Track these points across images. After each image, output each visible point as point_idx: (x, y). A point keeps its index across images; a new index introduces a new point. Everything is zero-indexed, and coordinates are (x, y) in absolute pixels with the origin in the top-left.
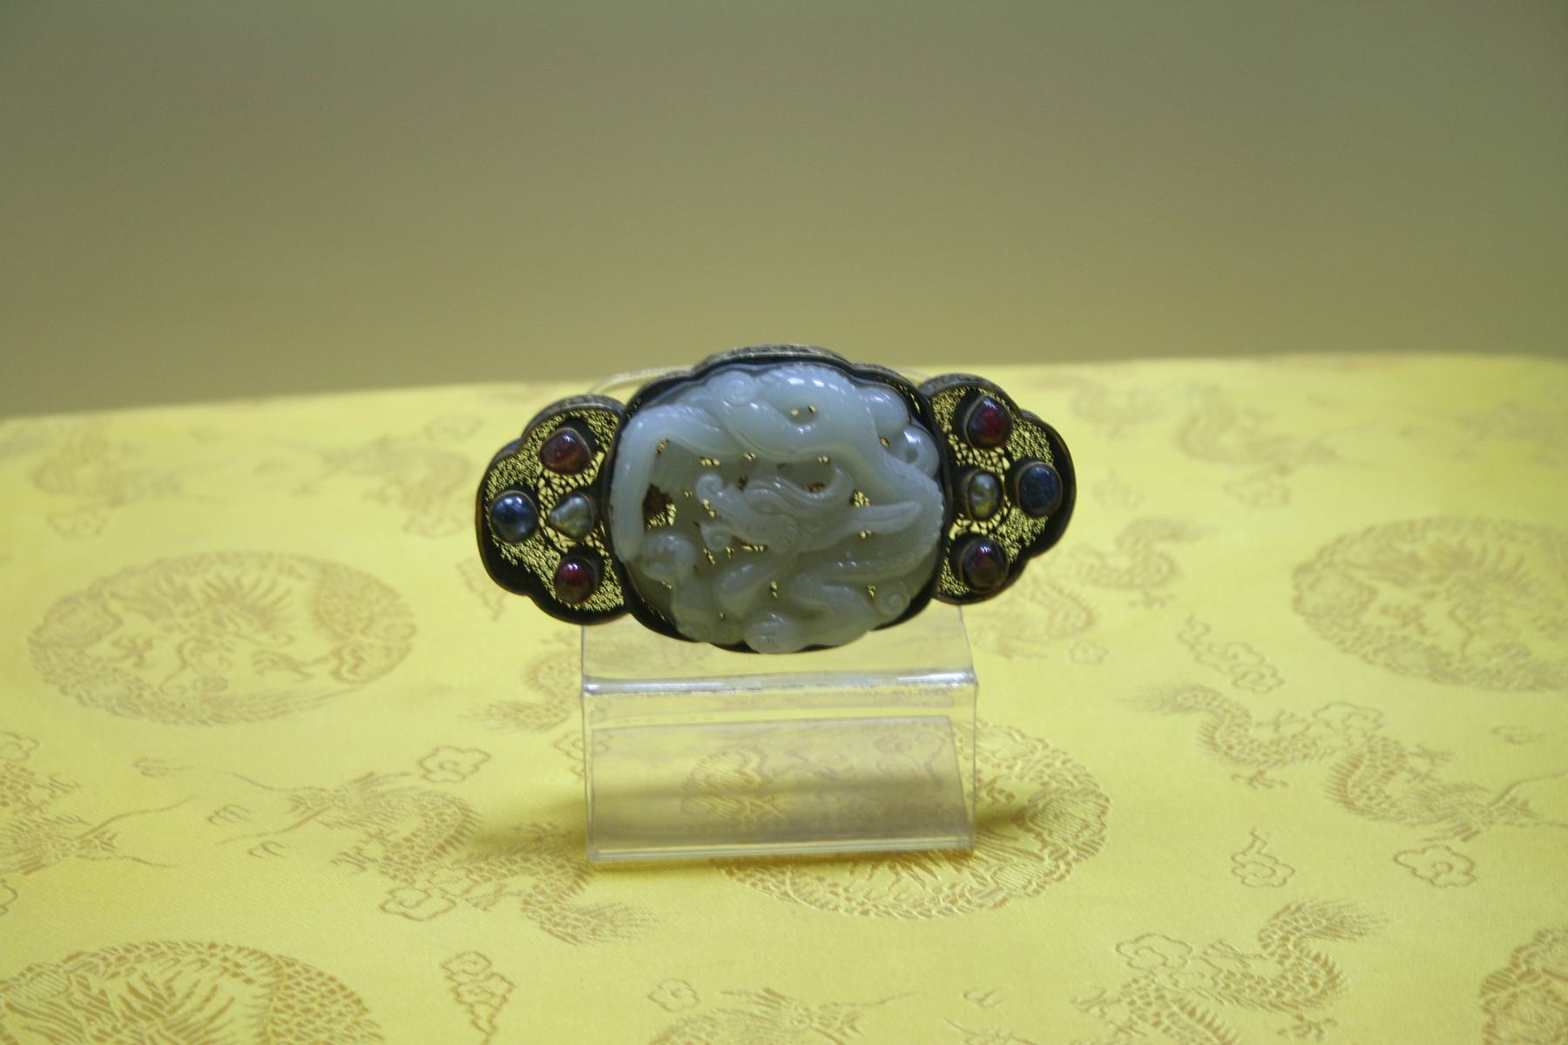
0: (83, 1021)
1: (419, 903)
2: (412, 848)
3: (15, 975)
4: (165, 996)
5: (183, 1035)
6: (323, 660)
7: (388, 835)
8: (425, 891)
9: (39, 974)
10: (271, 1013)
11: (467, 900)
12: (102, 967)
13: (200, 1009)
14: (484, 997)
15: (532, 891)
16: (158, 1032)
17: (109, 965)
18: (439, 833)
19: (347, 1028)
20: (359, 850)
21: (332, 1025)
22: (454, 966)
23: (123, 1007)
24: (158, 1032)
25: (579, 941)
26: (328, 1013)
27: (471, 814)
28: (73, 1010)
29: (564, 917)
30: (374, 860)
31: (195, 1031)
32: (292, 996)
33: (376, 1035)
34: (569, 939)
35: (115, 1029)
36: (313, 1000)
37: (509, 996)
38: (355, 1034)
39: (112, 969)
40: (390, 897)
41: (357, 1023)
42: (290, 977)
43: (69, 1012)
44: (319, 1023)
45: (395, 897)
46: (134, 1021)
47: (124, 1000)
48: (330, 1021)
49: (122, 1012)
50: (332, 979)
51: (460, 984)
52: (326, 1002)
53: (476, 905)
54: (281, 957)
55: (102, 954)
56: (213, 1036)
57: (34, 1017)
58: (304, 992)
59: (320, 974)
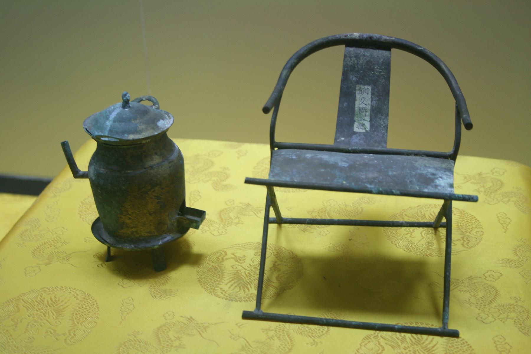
0: (400, 343)
1: (486, 318)
2: (483, 301)
3: (407, 209)
4: (421, 339)
5: (426, 351)
6: (459, 240)
7: (476, 296)
8: (493, 199)
9: (412, 209)
10: (460, 221)
11: (499, 319)
12: (425, 209)
13: (429, 344)
14: (504, 349)
15: (516, 318)
16: (419, 349)
17: (426, 208)
18: (490, 297)
19: (476, 226)
20: (479, 189)
21: (473, 225)
22: (499, 215)
23: (410, 341)
24: (419, 349)
25: (529, 336)
26: (472, 222)
27: (498, 292)
28: (397, 340)
29: (525, 328)
30: (482, 192)
31: (429, 350)
32: (464, 218)
33: (481, 227)
34: (526, 334)
35: (408, 346)
36: (468, 219)
37: (511, 350)
38: (477, 227)
39: (427, 209)
40: (478, 315)
41: (478, 225)
42: (464, 214)
43: (396, 340)
44: (470, 224)
45: (479, 315)
46: (413, 345)
47: (429, 216)
48: (473, 224)
49: (429, 219)
50: (472, 215)
51: (500, 219)
52: (462, 346)
53: (504, 203)
54: (462, 210)
55: (425, 206)
56: (433, 352)
57: (410, 218)
58: (466, 218)
59: (470, 214)
